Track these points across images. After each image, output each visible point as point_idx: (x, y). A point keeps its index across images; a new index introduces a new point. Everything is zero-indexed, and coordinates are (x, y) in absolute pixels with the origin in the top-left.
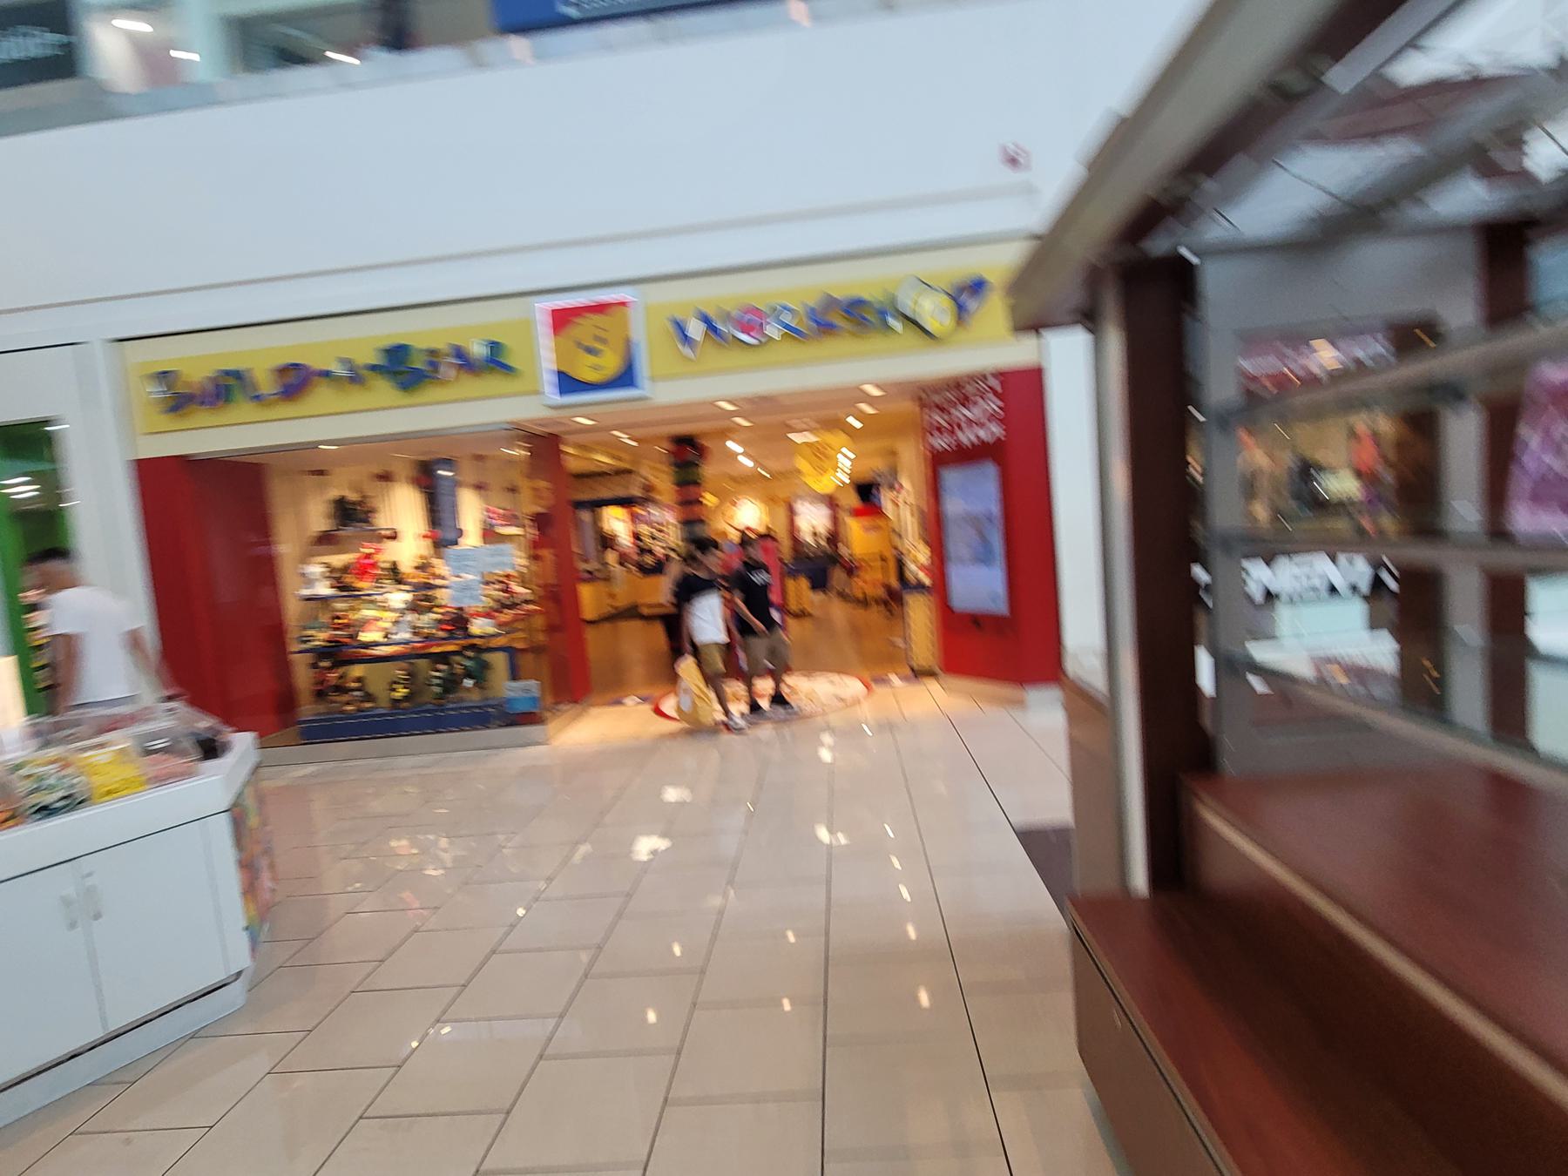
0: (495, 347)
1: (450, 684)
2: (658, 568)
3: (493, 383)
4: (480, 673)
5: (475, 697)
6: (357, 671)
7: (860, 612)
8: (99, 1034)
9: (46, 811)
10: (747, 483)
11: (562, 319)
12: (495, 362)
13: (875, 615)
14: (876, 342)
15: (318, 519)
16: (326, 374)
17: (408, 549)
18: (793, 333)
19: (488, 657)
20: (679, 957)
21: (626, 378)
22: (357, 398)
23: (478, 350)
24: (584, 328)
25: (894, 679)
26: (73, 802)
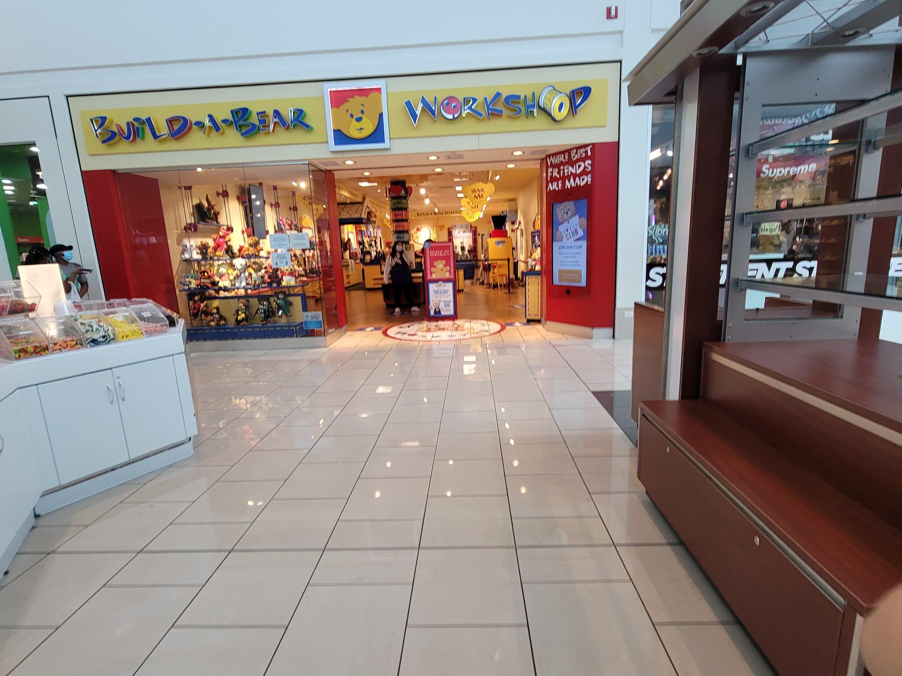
0: (299, 113)
1: (269, 314)
2: (379, 259)
3: (298, 135)
4: (287, 307)
5: (284, 321)
6: (216, 303)
7: (492, 292)
8: (126, 459)
9: (94, 342)
10: (427, 215)
11: (338, 99)
12: (299, 121)
13: (501, 293)
14: (523, 123)
15: (187, 216)
16: (200, 124)
17: (238, 240)
18: (476, 114)
19: (291, 299)
20: (389, 468)
21: (377, 135)
22: (215, 139)
23: (289, 115)
24: (354, 104)
25: (517, 324)
26: (107, 339)
